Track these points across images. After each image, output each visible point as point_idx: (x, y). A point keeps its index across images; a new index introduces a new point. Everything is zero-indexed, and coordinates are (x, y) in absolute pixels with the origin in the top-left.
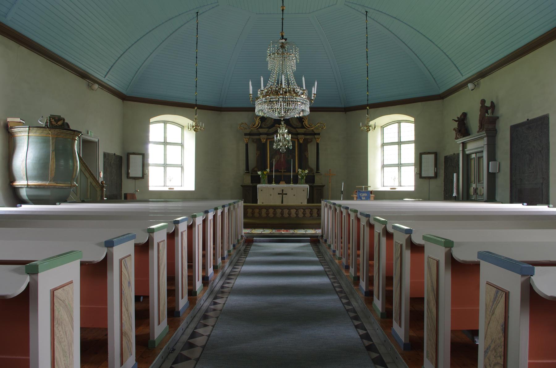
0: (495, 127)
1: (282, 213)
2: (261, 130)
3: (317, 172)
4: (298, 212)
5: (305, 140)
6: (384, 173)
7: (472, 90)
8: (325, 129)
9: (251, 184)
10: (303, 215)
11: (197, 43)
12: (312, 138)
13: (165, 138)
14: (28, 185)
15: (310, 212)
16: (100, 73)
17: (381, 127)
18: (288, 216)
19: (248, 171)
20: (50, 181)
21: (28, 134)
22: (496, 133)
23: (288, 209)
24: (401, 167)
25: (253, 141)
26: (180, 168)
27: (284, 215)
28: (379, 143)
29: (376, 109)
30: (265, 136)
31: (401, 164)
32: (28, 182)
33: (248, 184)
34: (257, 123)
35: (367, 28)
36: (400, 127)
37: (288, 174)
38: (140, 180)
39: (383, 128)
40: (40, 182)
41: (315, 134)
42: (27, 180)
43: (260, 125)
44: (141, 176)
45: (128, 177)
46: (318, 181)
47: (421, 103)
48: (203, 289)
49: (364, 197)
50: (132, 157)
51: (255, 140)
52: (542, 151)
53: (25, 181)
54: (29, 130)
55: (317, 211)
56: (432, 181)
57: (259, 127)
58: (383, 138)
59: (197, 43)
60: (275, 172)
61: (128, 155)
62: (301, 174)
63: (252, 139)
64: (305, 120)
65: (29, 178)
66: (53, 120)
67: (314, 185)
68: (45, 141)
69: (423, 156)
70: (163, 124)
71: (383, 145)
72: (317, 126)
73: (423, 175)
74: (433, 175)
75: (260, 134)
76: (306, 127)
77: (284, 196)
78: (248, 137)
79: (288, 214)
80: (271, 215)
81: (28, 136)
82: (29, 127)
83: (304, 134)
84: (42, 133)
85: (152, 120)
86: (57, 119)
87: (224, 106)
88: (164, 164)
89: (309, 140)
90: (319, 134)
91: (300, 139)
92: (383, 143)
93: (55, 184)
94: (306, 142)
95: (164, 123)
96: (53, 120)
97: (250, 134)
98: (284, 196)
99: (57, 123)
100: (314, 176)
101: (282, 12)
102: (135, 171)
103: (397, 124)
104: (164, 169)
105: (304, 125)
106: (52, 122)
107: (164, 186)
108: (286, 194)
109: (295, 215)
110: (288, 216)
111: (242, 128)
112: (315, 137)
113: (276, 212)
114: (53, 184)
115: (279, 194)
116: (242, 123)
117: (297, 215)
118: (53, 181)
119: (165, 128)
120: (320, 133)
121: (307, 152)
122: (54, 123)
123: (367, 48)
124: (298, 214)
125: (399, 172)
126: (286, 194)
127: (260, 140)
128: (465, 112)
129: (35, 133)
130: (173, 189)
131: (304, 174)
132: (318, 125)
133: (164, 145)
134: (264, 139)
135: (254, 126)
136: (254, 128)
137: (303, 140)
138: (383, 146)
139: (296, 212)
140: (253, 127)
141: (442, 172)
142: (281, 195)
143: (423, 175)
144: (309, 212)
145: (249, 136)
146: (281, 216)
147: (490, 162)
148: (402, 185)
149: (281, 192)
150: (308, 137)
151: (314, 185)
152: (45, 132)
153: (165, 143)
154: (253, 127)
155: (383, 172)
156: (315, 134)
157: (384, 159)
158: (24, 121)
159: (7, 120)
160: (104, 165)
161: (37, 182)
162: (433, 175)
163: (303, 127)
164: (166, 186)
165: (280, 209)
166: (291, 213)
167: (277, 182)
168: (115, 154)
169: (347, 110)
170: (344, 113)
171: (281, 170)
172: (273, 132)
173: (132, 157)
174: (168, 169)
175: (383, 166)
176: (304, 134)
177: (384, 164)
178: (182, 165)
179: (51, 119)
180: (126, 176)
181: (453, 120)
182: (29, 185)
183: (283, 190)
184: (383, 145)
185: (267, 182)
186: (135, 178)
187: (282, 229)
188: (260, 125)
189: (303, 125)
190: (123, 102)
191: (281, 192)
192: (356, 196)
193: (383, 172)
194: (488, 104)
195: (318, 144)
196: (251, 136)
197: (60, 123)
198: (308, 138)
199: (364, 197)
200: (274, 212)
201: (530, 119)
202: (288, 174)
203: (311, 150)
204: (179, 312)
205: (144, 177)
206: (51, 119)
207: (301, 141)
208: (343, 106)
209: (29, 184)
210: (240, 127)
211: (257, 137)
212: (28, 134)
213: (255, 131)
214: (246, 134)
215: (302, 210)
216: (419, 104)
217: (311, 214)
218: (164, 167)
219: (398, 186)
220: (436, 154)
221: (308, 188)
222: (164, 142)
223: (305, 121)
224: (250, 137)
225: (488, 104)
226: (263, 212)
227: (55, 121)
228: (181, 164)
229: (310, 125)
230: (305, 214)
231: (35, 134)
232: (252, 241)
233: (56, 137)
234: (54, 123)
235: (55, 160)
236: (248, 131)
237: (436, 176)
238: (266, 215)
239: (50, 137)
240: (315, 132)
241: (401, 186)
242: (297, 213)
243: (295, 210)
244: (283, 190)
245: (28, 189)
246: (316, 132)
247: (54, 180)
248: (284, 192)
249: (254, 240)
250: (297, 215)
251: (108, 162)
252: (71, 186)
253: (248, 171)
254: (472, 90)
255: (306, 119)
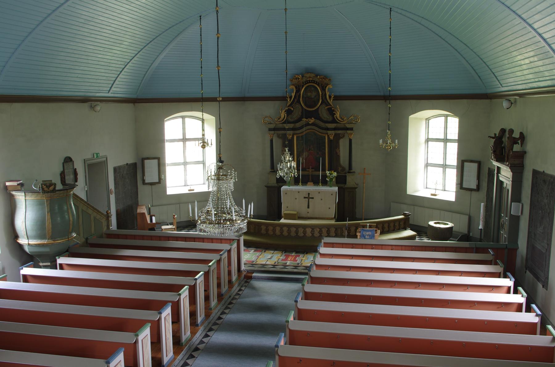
0: (523, 162)
1: (297, 232)
2: (287, 126)
3: (349, 172)
4: (314, 231)
5: (336, 135)
6: (428, 173)
7: (507, 109)
8: (359, 122)
9: (276, 185)
10: (319, 235)
11: (201, 51)
12: (345, 133)
13: (184, 134)
14: (29, 244)
15: (327, 231)
16: (102, 92)
17: (426, 119)
18: (303, 235)
19: (273, 170)
20: (49, 239)
21: (25, 197)
22: (523, 169)
23: (303, 228)
24: (445, 168)
25: (278, 136)
26: (202, 165)
27: (299, 234)
28: (423, 138)
29: (419, 101)
30: (291, 132)
31: (446, 165)
32: (29, 241)
33: (273, 185)
34: (282, 116)
35: (390, 28)
36: (447, 122)
37: (316, 173)
38: (157, 185)
39: (428, 120)
40: (39, 241)
41: (348, 129)
42: (28, 239)
43: (285, 118)
44: (157, 181)
45: (144, 183)
46: (351, 181)
47: (466, 100)
48: (218, 304)
49: (368, 235)
50: (146, 162)
51: (280, 136)
52: (550, 214)
53: (26, 240)
54: (25, 194)
55: (335, 231)
56: (474, 193)
57: (284, 122)
58: (428, 133)
59: (201, 51)
60: (301, 171)
61: (143, 160)
62: (329, 177)
63: (277, 134)
64: (336, 112)
65: (29, 238)
66: (45, 186)
67: (346, 186)
68: (40, 204)
69: (466, 164)
70: (181, 119)
71: (428, 140)
72: (350, 118)
73: (465, 186)
74: (475, 187)
75: (284, 129)
76: (338, 121)
77: (310, 200)
78: (273, 132)
79: (302, 234)
80: (285, 233)
81: (25, 199)
82: (25, 193)
83: (335, 129)
84: (36, 196)
85: (165, 120)
86: (48, 185)
87: (247, 95)
88: (184, 162)
89: (341, 136)
90: (351, 129)
91: (330, 135)
92: (428, 138)
93: (53, 242)
94: (338, 137)
95: (182, 118)
96: (45, 186)
97: (274, 129)
98: (310, 200)
99: (48, 189)
100: (346, 176)
101: (219, 133)
102: (151, 176)
103: (444, 118)
104: (184, 168)
105: (335, 117)
106: (44, 188)
107: (185, 186)
108: (313, 198)
109: (311, 235)
110: (303, 235)
111: (266, 122)
112: (347, 132)
113: (290, 231)
114: (51, 241)
115: (305, 198)
116: (266, 117)
117: (313, 234)
118: (51, 239)
119: (184, 123)
120: (353, 128)
121: (339, 148)
122: (46, 189)
123: (390, 52)
124: (314, 233)
125: (443, 173)
126: (313, 198)
127: (285, 134)
128: (504, 128)
129: (30, 196)
130: (193, 190)
131: (332, 176)
132: (351, 118)
133: (183, 142)
134: (290, 135)
135: (280, 120)
136: (279, 121)
137: (333, 136)
138: (428, 142)
139: (312, 231)
140: (279, 120)
141: (484, 185)
142: (307, 199)
143: (464, 186)
144: (326, 231)
145: (274, 131)
146: (295, 235)
147: (512, 203)
148: (446, 189)
149: (307, 196)
150: (339, 132)
151: (346, 186)
152: (39, 195)
153: (184, 140)
154: (279, 120)
155: (427, 172)
156: (348, 129)
157: (428, 157)
158: (21, 180)
159: (6, 184)
160: (115, 180)
161: (35, 241)
162: (475, 187)
163: (334, 121)
164: (187, 186)
165: (295, 227)
166: (306, 233)
167: (305, 183)
168: (127, 164)
169: (387, 98)
170: (383, 101)
171: (309, 170)
172: (300, 126)
173: (146, 162)
174: (188, 166)
175: (427, 165)
176: (335, 129)
177: (429, 162)
178: (203, 161)
179: (43, 186)
180: (142, 182)
181: (489, 137)
182: (30, 244)
183: (309, 194)
184: (428, 140)
185: (293, 183)
186: (152, 184)
187: (292, 252)
188: (285, 118)
189: (335, 118)
190: (134, 105)
191: (307, 196)
192: (360, 234)
193: (427, 172)
194: (516, 135)
195: (350, 141)
196: (276, 131)
197: (51, 188)
198: (339, 133)
199: (368, 235)
200: (288, 230)
201: (545, 172)
202: (316, 173)
203: (343, 145)
204: (182, 343)
205: (160, 182)
206: (43, 186)
207: (332, 138)
208: (382, 94)
209: (30, 243)
210: (264, 121)
211: (283, 132)
212: (24, 197)
213: (281, 126)
214: (270, 130)
215: (318, 230)
216: (465, 101)
217: (328, 233)
218: (184, 165)
219: (442, 190)
220: (479, 164)
221: (336, 192)
222: (183, 139)
223: (336, 113)
224: (274, 132)
225: (516, 135)
226: (277, 230)
227: (47, 187)
228: (202, 160)
229: (342, 119)
230: (322, 233)
231: (31, 197)
232: (251, 278)
233: (50, 199)
234: (46, 189)
235: (50, 221)
236: (272, 126)
237: (478, 188)
238: (280, 234)
239: (44, 199)
240: (348, 127)
241: (445, 190)
242: (312, 232)
243: (311, 230)
244: (309, 194)
245: (29, 247)
246: (348, 126)
247: (52, 238)
248: (310, 196)
249: (252, 277)
250: (313, 234)
251: (120, 175)
252: (68, 240)
253: (273, 170)
254: (507, 109)
255: (338, 112)
